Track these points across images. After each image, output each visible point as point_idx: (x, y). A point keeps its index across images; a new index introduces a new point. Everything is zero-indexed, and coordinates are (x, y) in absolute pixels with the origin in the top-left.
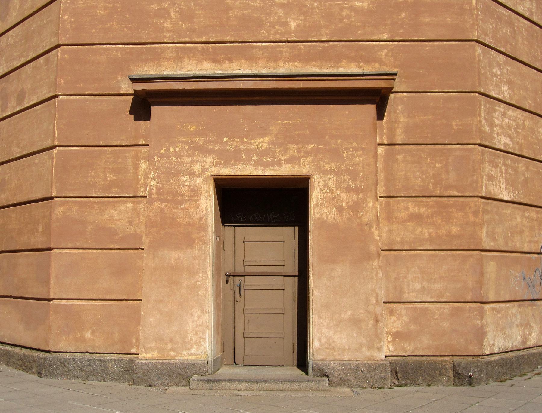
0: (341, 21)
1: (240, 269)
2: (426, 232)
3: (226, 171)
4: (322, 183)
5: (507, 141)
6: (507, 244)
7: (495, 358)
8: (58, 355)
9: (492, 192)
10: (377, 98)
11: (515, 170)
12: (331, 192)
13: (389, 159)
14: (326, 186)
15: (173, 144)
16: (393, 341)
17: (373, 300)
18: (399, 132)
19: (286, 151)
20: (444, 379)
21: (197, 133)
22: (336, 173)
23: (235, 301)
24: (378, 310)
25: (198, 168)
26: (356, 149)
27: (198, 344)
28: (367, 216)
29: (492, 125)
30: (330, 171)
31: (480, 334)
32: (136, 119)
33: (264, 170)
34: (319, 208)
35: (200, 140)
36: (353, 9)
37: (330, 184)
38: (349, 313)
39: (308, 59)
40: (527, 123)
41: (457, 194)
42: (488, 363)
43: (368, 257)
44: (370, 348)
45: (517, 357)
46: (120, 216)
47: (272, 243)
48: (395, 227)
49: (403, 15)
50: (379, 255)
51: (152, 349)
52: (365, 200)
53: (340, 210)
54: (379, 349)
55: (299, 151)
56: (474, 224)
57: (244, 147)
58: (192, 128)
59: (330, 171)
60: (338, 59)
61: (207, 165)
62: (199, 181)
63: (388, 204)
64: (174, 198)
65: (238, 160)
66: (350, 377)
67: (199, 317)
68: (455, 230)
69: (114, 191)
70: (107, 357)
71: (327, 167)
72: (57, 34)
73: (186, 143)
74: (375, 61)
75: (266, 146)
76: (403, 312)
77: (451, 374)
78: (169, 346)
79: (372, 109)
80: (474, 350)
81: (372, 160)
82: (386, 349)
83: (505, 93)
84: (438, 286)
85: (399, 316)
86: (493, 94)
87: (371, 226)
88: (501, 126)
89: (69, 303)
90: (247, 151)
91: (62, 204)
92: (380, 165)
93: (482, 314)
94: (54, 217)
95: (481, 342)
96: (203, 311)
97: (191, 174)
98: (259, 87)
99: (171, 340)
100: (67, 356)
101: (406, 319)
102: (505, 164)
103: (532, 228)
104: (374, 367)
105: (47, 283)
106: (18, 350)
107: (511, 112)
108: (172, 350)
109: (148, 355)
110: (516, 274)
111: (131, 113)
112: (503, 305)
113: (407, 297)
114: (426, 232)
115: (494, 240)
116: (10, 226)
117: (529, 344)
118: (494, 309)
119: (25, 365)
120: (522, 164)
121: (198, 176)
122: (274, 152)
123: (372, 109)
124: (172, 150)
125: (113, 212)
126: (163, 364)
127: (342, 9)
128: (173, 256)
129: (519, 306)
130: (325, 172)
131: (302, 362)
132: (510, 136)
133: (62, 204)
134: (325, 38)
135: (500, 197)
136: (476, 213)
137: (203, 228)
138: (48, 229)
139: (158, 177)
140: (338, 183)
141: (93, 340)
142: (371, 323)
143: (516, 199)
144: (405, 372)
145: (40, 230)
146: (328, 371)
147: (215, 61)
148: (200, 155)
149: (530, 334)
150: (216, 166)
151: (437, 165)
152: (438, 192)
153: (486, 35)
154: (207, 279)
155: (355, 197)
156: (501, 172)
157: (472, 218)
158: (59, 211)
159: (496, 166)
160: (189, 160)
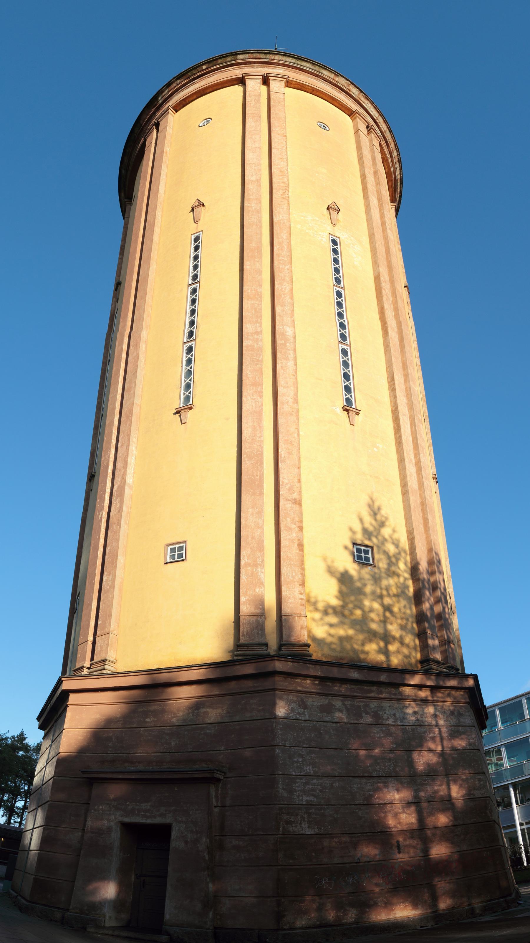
3: (127, 820)
4: (177, 828)
9: (292, 831)
33: (146, 820)
34: (176, 842)
37: (181, 828)
41: (262, 833)
49: (233, 736)
53: (186, 842)
55: (166, 811)
71: (180, 819)
75: (149, 807)
121: (112, 821)
134: (190, 750)
150: (122, 816)
151: (250, 817)
160: (108, 813)
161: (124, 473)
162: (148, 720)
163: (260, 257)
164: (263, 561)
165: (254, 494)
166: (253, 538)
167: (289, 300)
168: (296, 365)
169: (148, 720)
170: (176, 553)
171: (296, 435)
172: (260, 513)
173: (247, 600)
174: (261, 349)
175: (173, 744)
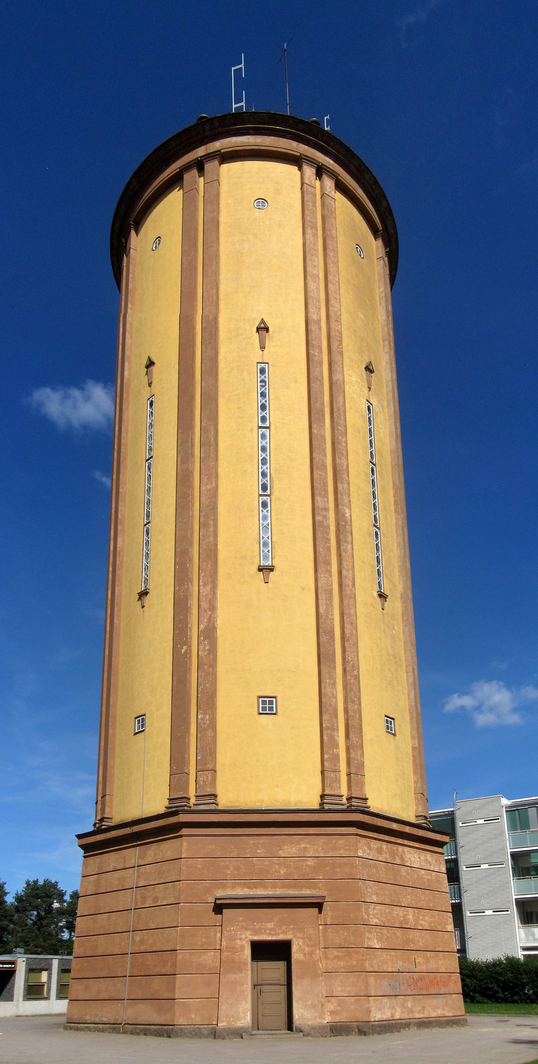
0: (302, 870)
1: (260, 982)
2: (342, 964)
3: (256, 938)
5: (377, 921)
6: (379, 968)
7: (377, 1023)
8: (179, 1027)
10: (319, 906)
11: (382, 933)
12: (301, 947)
13: (325, 931)
14: (298, 944)
15: (233, 926)
16: (330, 1015)
17: (320, 995)
18: (328, 919)
19: (281, 929)
20: (354, 1033)
21: (243, 921)
22: (302, 938)
23: (258, 998)
24: (323, 1000)
25: (244, 936)
26: (310, 928)
27: (245, 1018)
28: (316, 957)
29: (368, 915)
30: (300, 938)
31: (369, 1011)
32: (215, 914)
34: (296, 954)
35: (244, 924)
36: (307, 865)
38: (310, 1002)
39: (289, 887)
40: (387, 911)
42: (373, 1025)
43: (317, 976)
44: (320, 1018)
45: (389, 1024)
46: (209, 958)
47: (274, 969)
48: (328, 961)
50: (322, 975)
51: (224, 1022)
52: (315, 950)
53: (305, 954)
54: (324, 1019)
56: (362, 960)
57: (263, 927)
58: (241, 919)
59: (300, 938)
60: (301, 887)
61: (248, 935)
62: (244, 942)
63: (325, 951)
64: (233, 950)
65: (261, 933)
66: (312, 1032)
67: (245, 1005)
68: (354, 963)
69: (205, 947)
70: (202, 1026)
72: (180, 875)
73: (238, 925)
74: (317, 888)
76: (334, 1001)
77: (357, 1030)
78: (232, 1019)
79: (316, 910)
80: (366, 1019)
81: (317, 933)
82: (327, 1019)
83: (375, 899)
84: (348, 989)
85: (332, 1003)
86: (368, 901)
87: (318, 962)
88: (373, 915)
89: (184, 1000)
90: (264, 929)
91: (182, 953)
92: (321, 934)
93: (368, 1002)
94: (178, 959)
95: (369, 1015)
96: (247, 1002)
97: (241, 939)
98: (293, 969)
99: (233, 1017)
100: (183, 1026)
101: (336, 1004)
102: (376, 932)
103: (392, 960)
104: (322, 1027)
105: (174, 991)
106: (152, 1027)
107: (378, 907)
108: (233, 1021)
109: (222, 1024)
110: (385, 983)
111: (213, 911)
112: (379, 998)
113: (335, 994)
114: (342, 964)
115: (372, 967)
116: (148, 963)
117: (395, 1018)
118: (374, 999)
119: (159, 1034)
120: (385, 931)
122: (276, 929)
123: (316, 910)
124: (232, 928)
125: (205, 957)
126: (229, 1028)
127: (302, 866)
128: (233, 977)
129: (388, 998)
130: (298, 938)
131: (290, 1026)
132: (378, 918)
133: (182, 953)
135: (374, 947)
136: (363, 955)
137: (246, 964)
138: (174, 965)
139: (226, 941)
140: (304, 943)
141: (195, 1018)
142: (320, 1006)
143: (383, 947)
144: (337, 1030)
145: (169, 965)
146: (302, 1029)
147: (249, 888)
148: (245, 931)
149: (395, 1012)
152: (346, 946)
153: (363, 875)
154: (248, 987)
155: (311, 949)
156: (374, 935)
157: (361, 957)
158: (180, 957)
159: (371, 933)
160: (239, 933)
161: (210, 616)
162: (259, 851)
163: (324, 423)
164: (338, 726)
165: (330, 667)
166: (331, 705)
167: (346, 477)
168: (352, 549)
169: (259, 851)
170: (267, 706)
171: (355, 618)
172: (334, 684)
173: (328, 758)
174: (328, 526)
175: (282, 872)
